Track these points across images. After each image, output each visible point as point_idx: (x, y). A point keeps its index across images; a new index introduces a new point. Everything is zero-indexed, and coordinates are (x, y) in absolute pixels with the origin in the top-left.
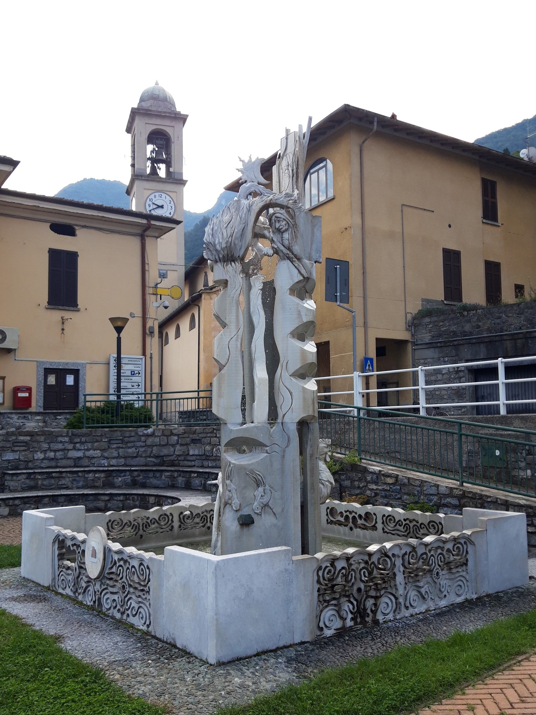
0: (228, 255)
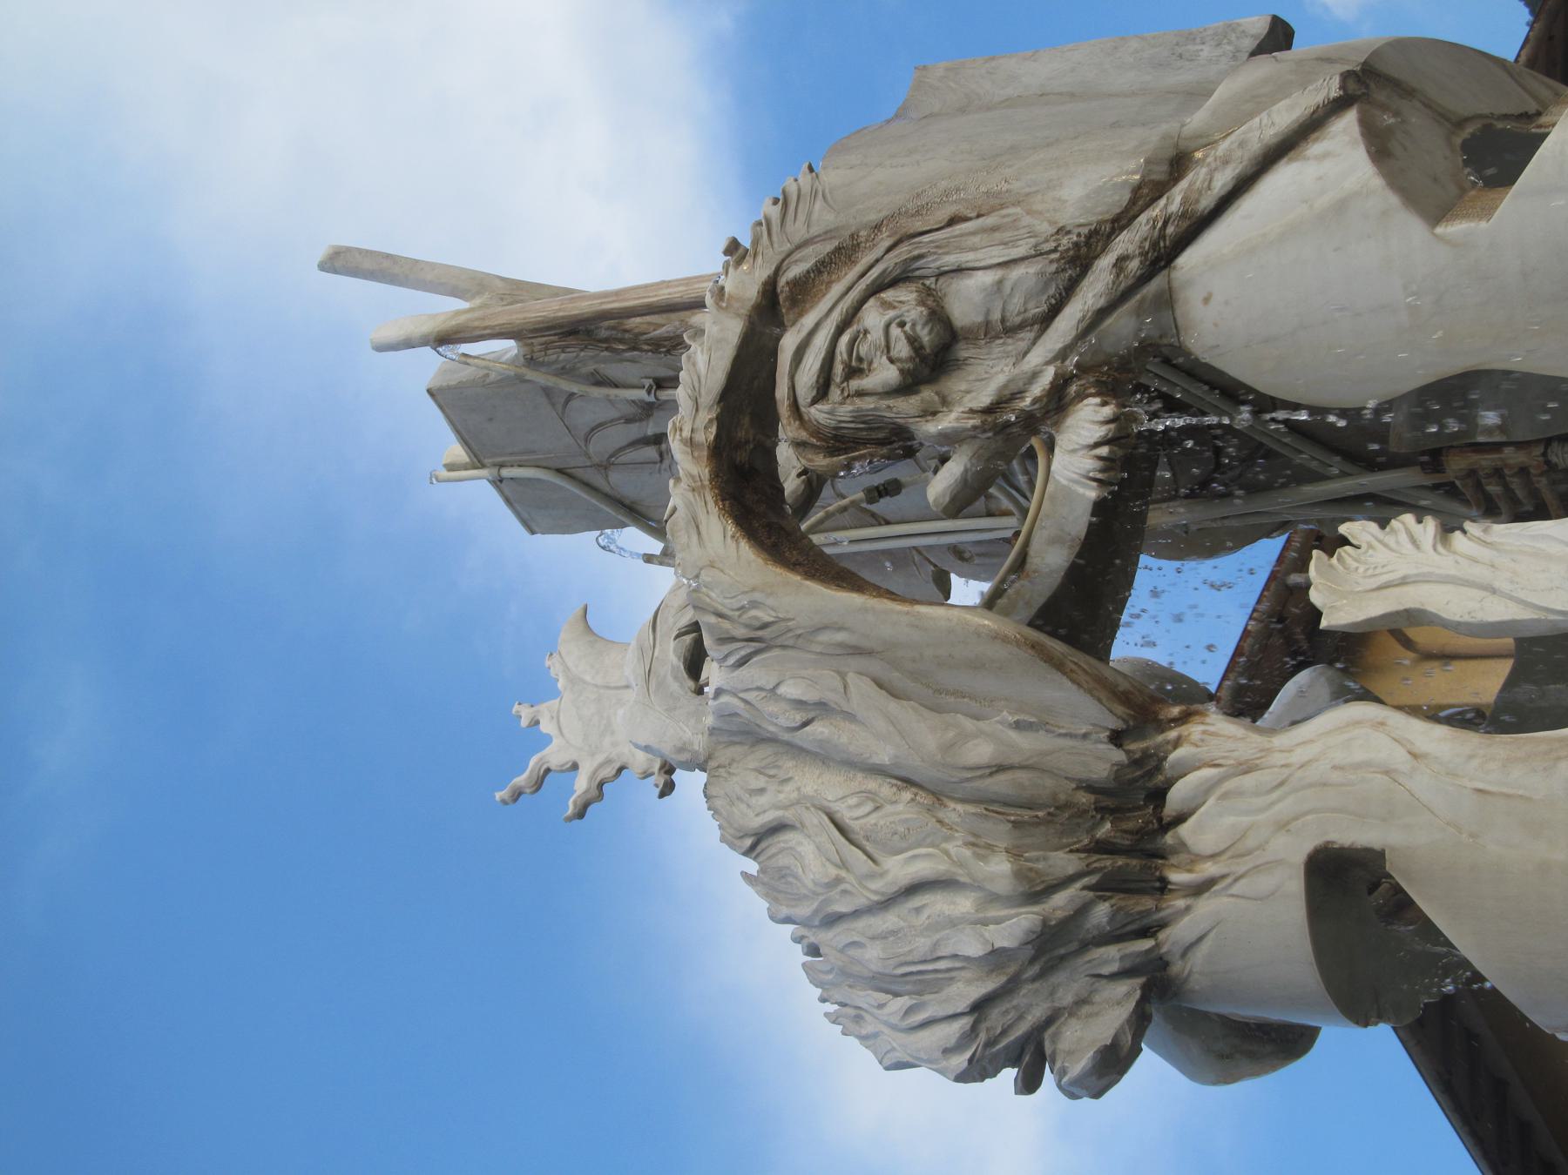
0: (1102, 848)
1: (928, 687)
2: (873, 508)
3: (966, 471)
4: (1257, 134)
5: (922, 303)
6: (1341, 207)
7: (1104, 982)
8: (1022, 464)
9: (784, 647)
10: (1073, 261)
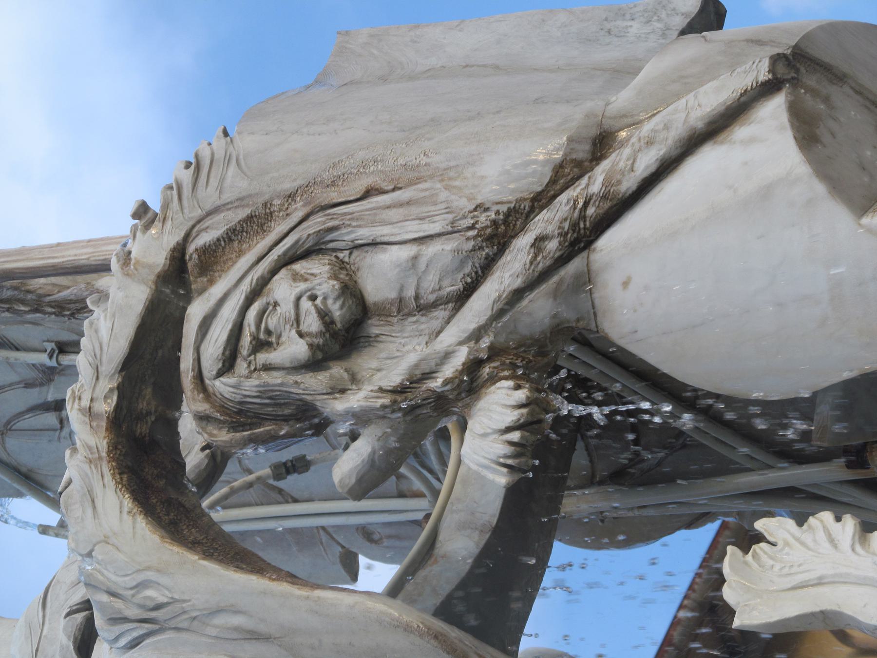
2: (281, 484)
3: (374, 452)
4: (683, 115)
5: (335, 277)
6: (766, 193)
8: (435, 444)
9: (177, 629)
10: (490, 239)
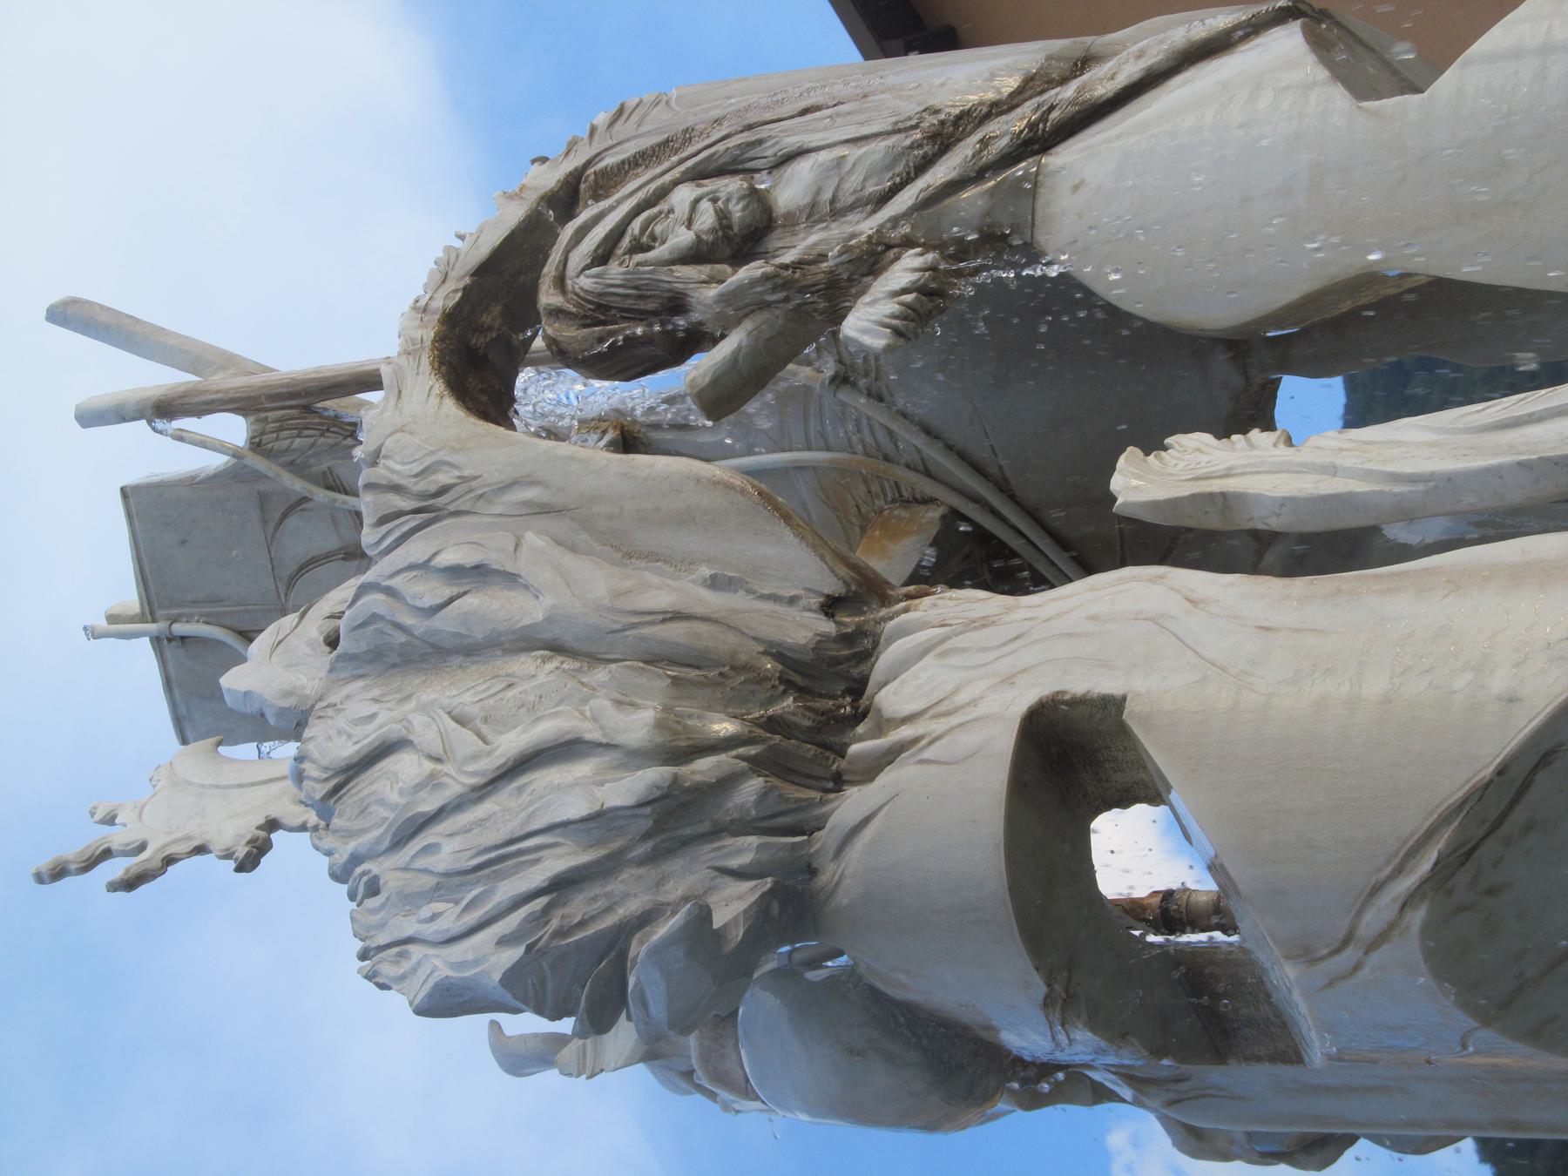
1: (618, 550)
7: (728, 879)
